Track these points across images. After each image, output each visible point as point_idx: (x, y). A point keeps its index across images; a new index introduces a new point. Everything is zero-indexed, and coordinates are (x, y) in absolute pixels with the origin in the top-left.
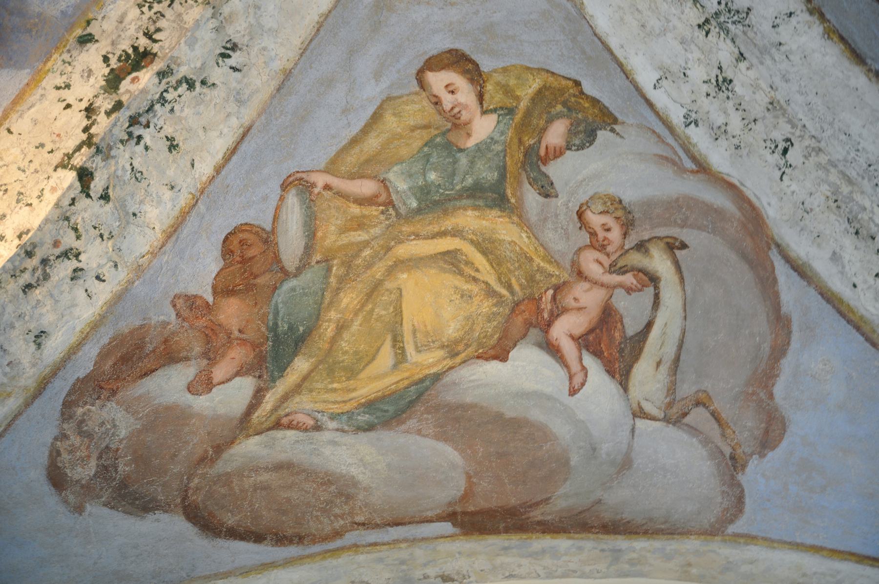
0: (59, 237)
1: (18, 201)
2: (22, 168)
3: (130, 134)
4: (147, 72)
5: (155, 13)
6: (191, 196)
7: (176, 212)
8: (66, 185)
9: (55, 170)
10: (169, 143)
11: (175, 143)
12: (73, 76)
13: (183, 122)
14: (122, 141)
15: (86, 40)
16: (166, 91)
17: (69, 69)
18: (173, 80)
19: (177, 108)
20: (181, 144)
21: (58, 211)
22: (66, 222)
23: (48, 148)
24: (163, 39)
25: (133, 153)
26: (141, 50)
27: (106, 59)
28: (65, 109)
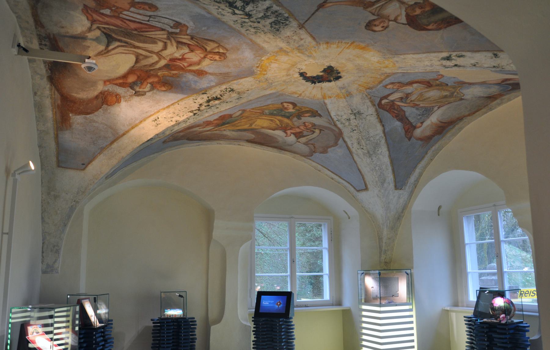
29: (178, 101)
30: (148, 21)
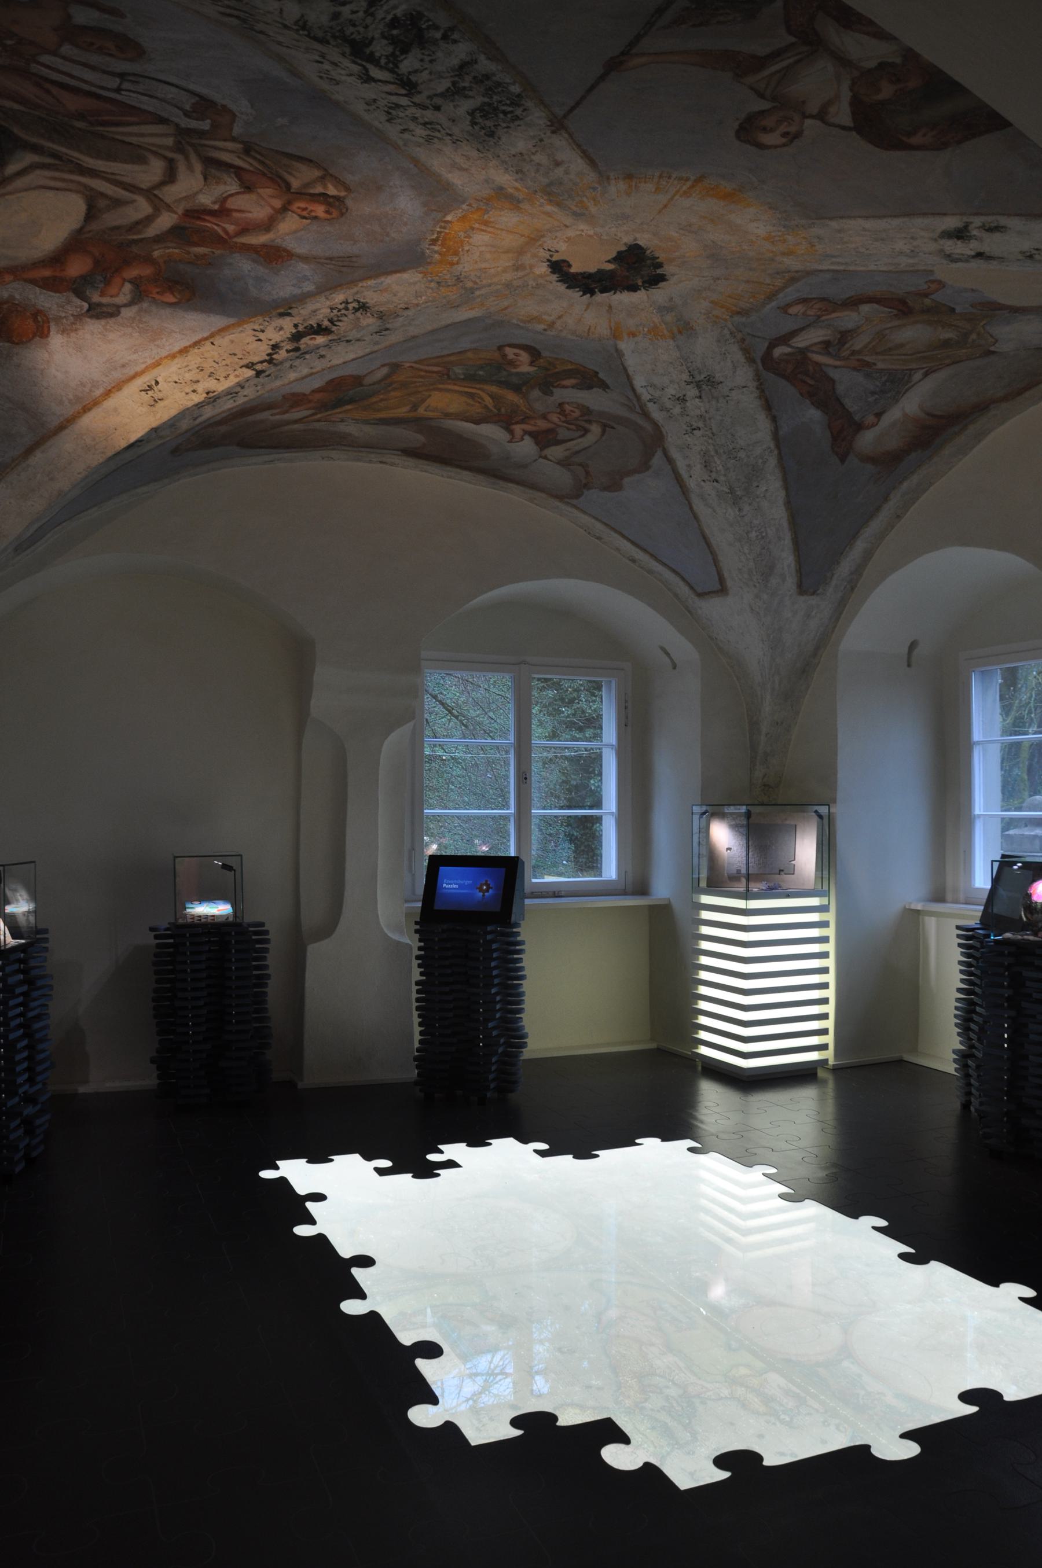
29: (212, 335)
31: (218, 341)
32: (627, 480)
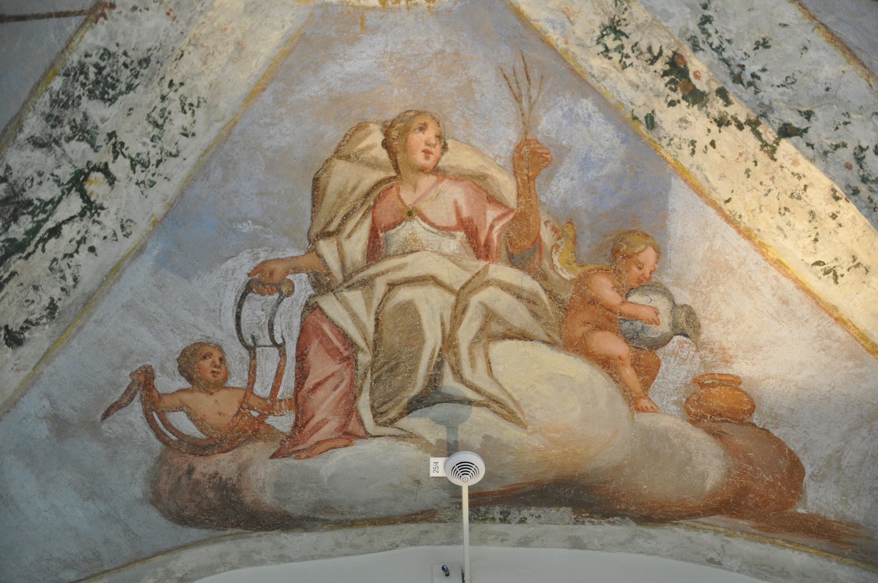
0: (843, 163)
1: (799, 198)
2: (766, 192)
3: (750, 84)
4: (691, 62)
5: (633, 52)
6: (816, 30)
7: (830, 47)
8: (792, 150)
9: (775, 160)
10: (761, 48)
11: (761, 41)
12: (683, 137)
13: (741, 31)
14: (756, 93)
15: (651, 122)
16: (711, 45)
17: (676, 140)
18: (701, 37)
19: (727, 36)
20: (763, 36)
21: (818, 160)
22: (829, 154)
23: (751, 165)
24: (659, 45)
25: (768, 83)
26: (667, 67)
27: (672, 104)
28: (714, 147)
29: (713, 204)
30: (281, 347)
31: (722, 190)
32: (613, 101)
